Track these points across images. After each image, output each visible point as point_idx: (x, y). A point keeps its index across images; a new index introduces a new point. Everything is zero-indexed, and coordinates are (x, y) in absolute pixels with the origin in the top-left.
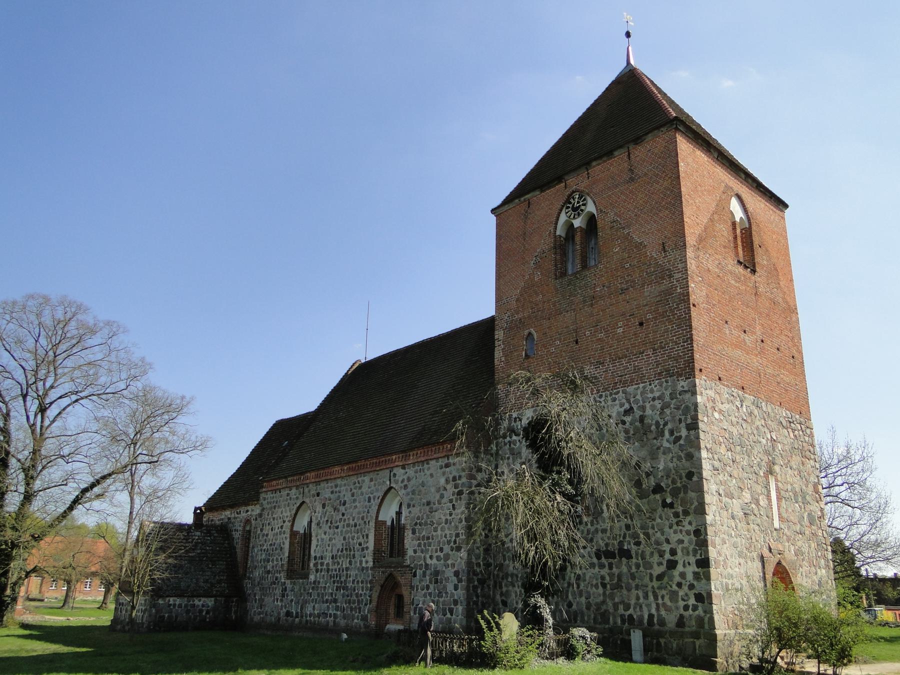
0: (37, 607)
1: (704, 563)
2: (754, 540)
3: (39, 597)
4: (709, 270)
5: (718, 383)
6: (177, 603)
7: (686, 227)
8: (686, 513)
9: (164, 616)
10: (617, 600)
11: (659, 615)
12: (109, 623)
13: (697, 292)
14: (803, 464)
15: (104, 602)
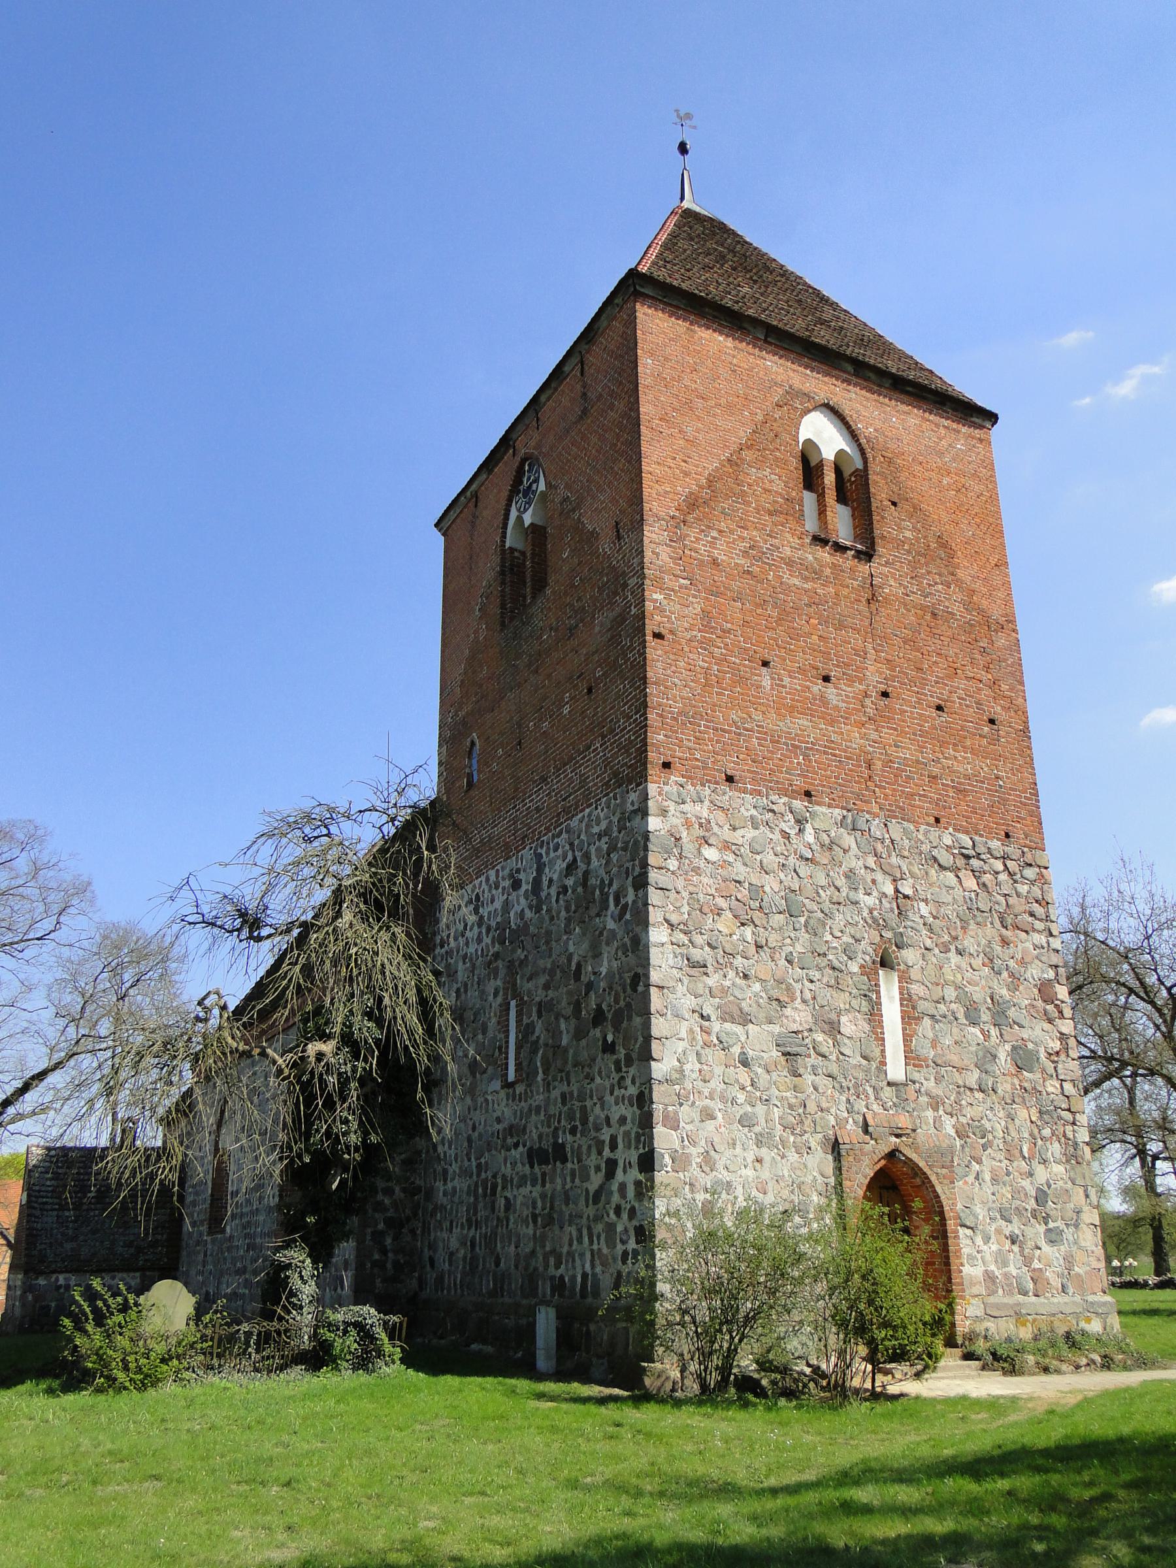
1: (648, 1162)
2: (812, 1107)
4: (715, 562)
5: (725, 787)
7: (646, 483)
8: (629, 1061)
9: (48, 1307)
10: (548, 1249)
11: (594, 1275)
13: (666, 603)
14: (1005, 942)
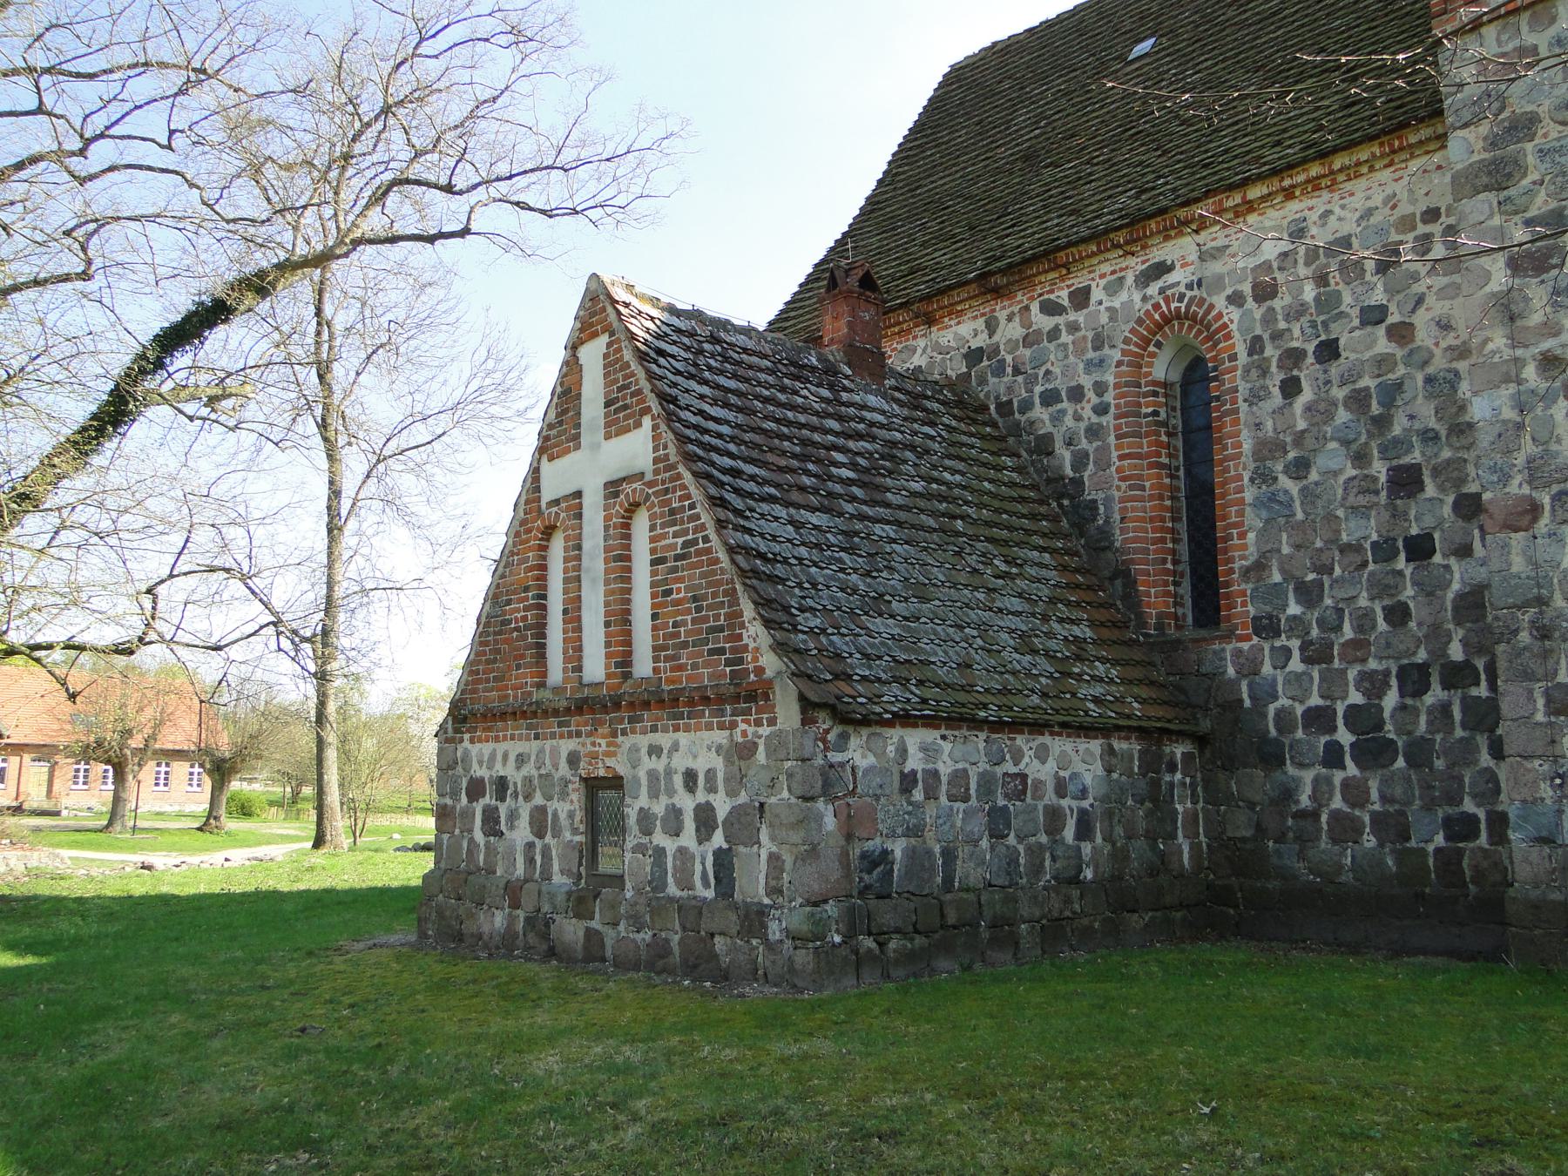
0: (37, 830)
3: (46, 805)
6: (945, 768)
9: (886, 854)
12: (416, 882)
15: (212, 814)
